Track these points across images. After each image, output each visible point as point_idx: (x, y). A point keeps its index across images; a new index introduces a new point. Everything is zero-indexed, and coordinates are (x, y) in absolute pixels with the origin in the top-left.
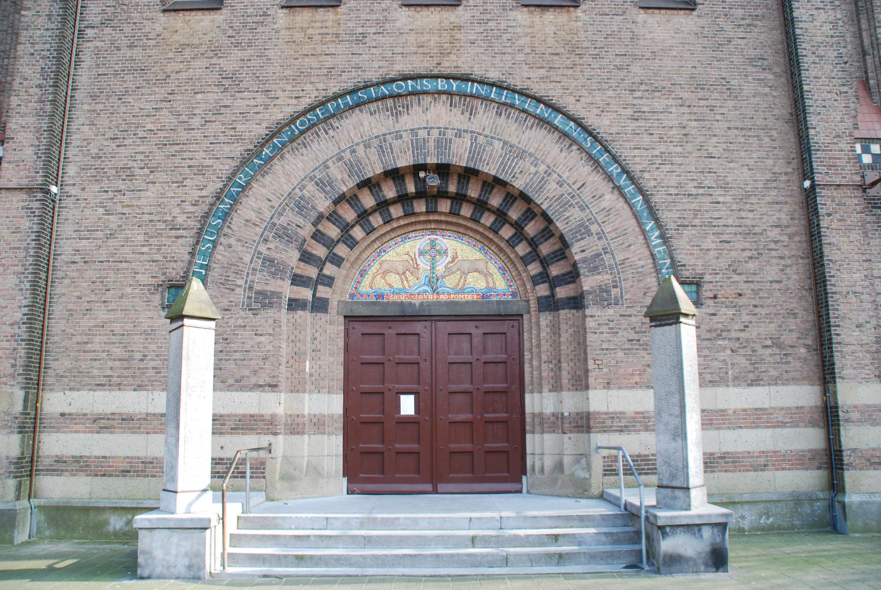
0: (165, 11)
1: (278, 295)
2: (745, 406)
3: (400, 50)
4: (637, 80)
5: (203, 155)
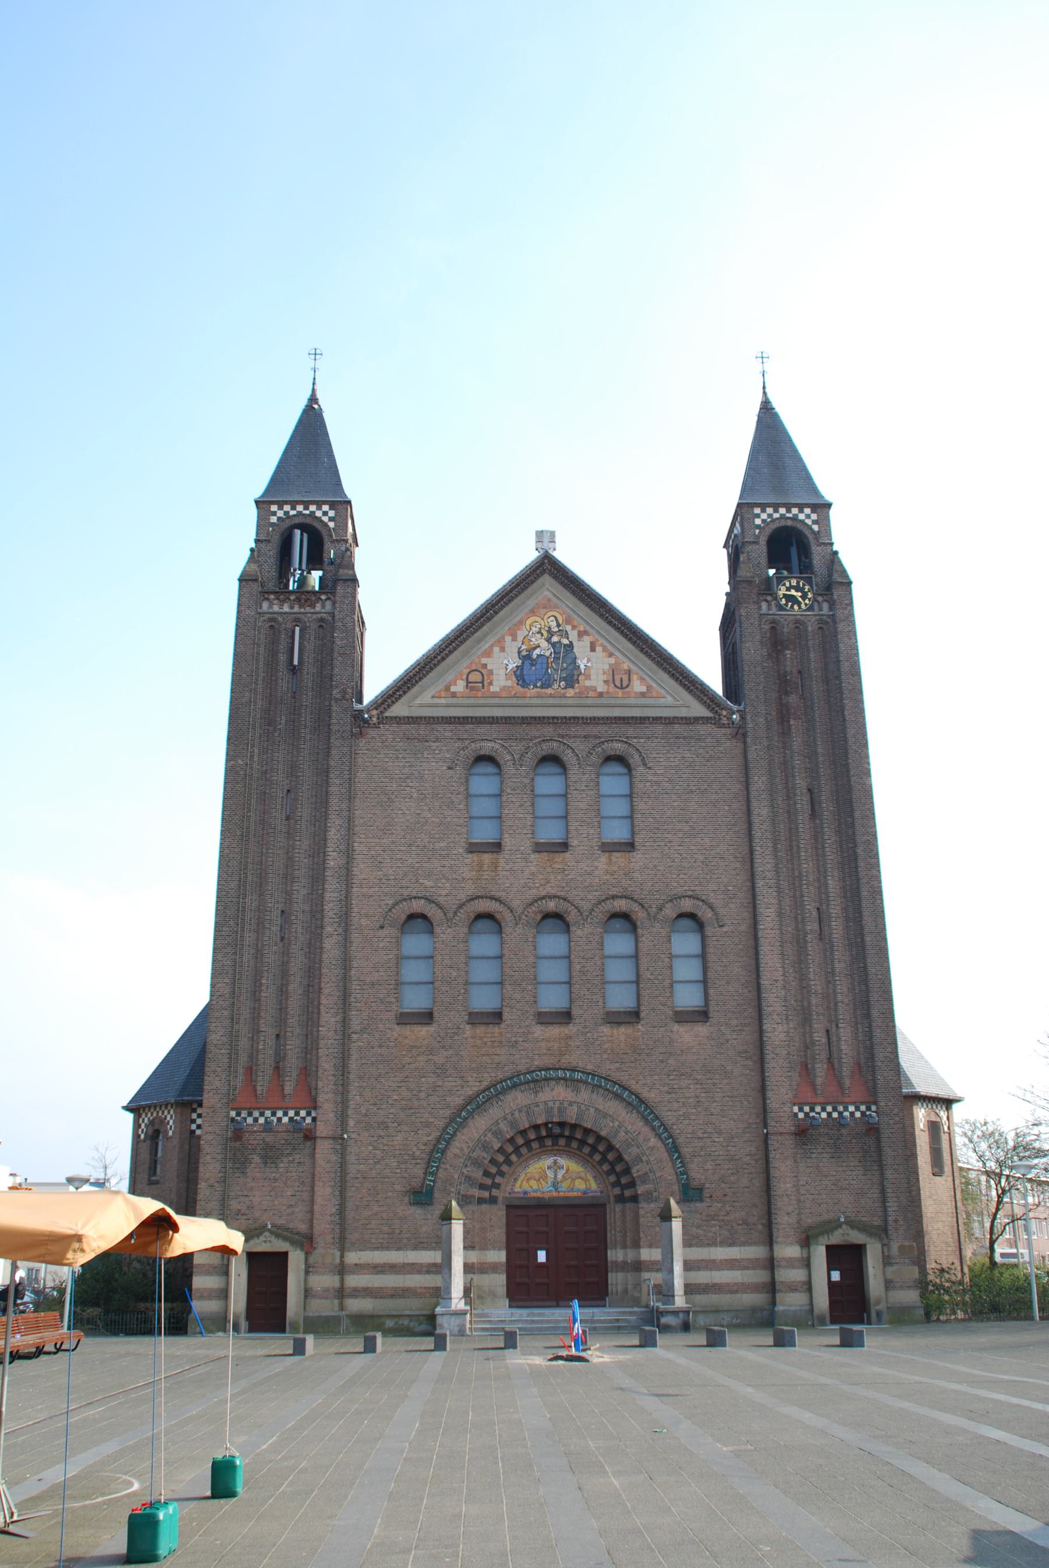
0: (398, 1024)
1: (473, 1196)
2: (726, 1258)
3: (537, 1052)
4: (672, 1068)
5: (428, 1115)
